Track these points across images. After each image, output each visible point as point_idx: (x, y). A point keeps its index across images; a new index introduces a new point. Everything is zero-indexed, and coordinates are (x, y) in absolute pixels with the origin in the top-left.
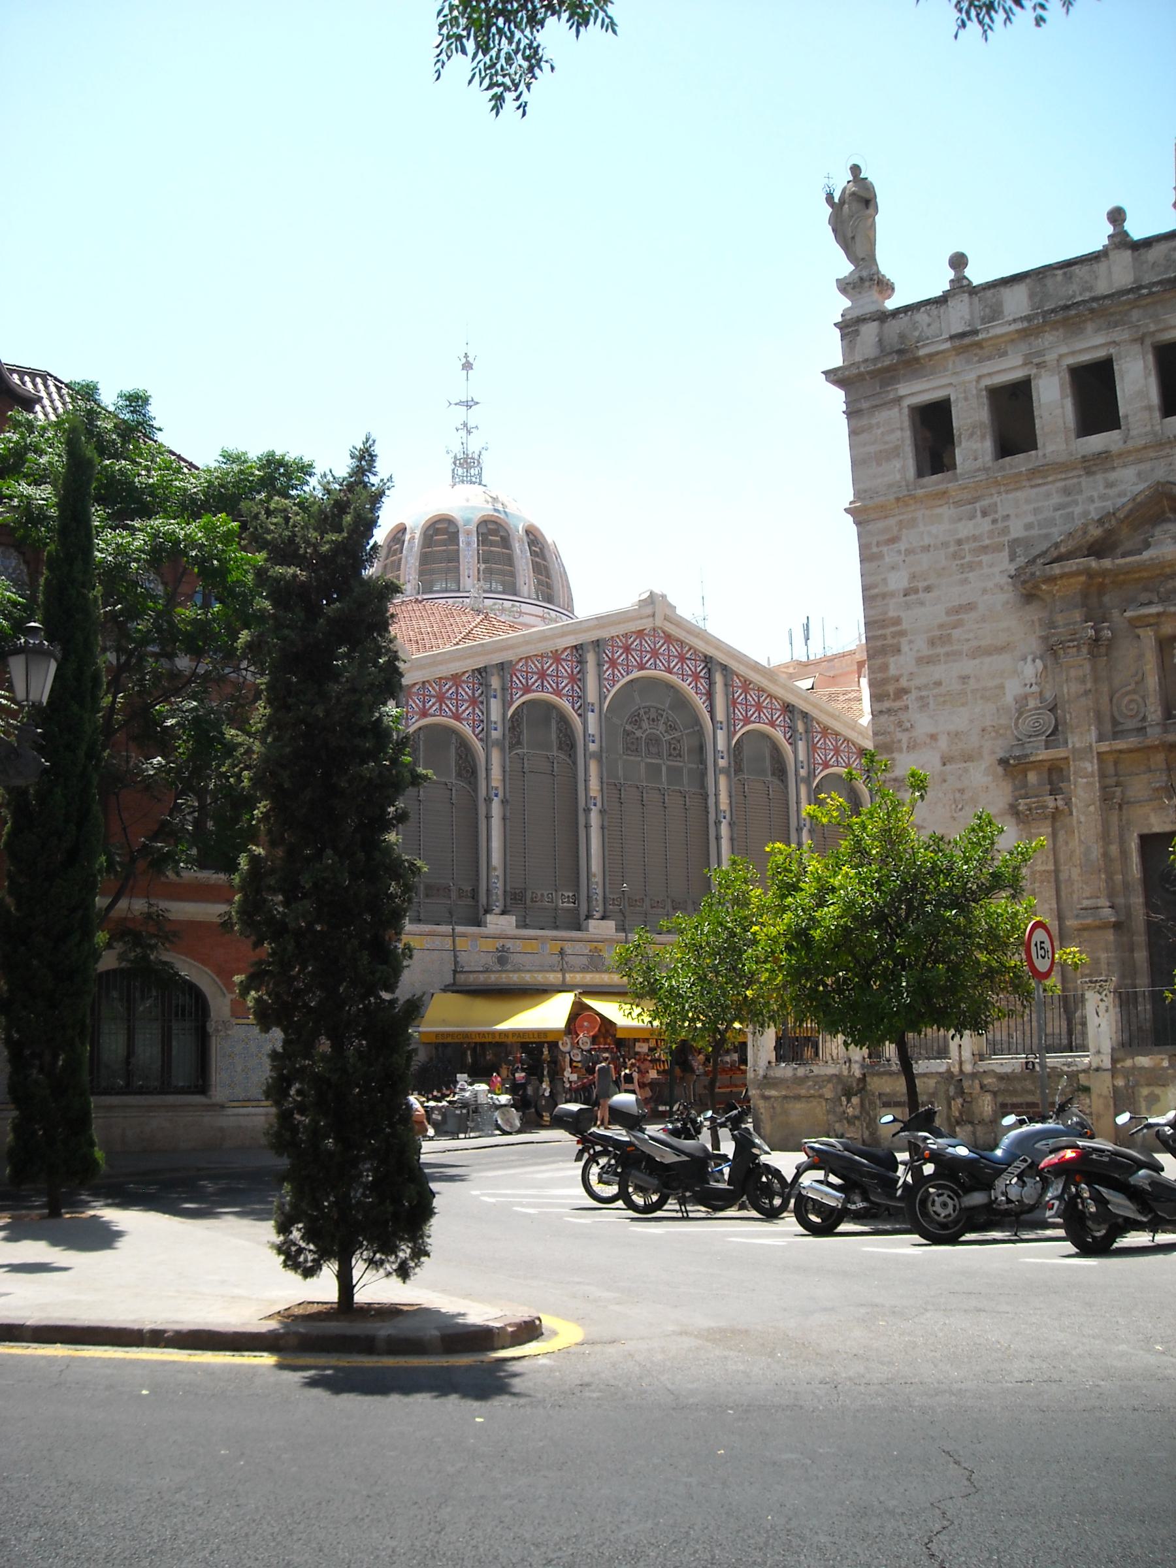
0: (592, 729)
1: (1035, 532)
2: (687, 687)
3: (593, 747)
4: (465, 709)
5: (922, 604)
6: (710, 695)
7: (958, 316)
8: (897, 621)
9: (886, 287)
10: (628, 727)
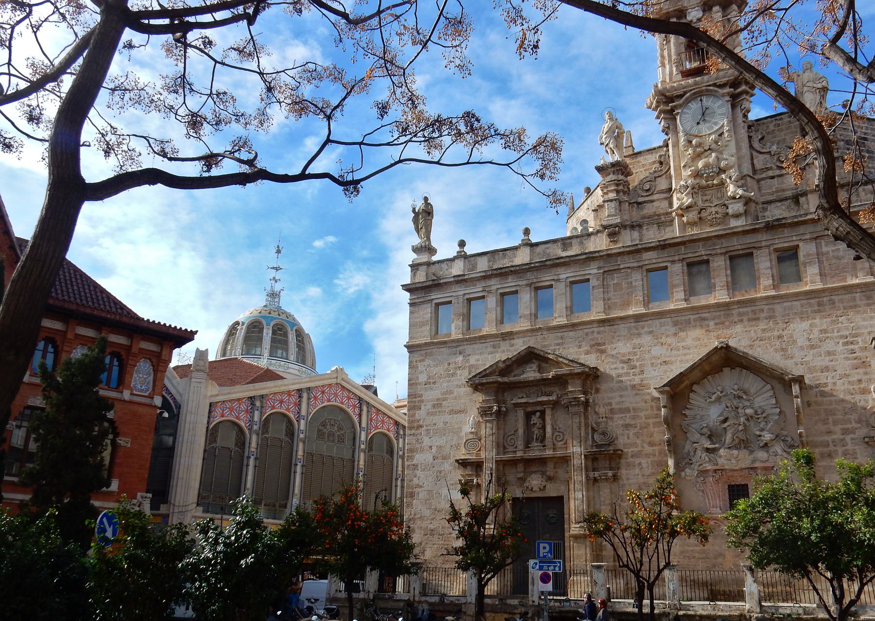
0: (302, 427)
1: (480, 363)
2: (350, 410)
3: (302, 436)
4: (243, 415)
5: (431, 389)
6: (360, 415)
7: (457, 269)
8: (421, 396)
9: (432, 251)
10: (320, 428)
